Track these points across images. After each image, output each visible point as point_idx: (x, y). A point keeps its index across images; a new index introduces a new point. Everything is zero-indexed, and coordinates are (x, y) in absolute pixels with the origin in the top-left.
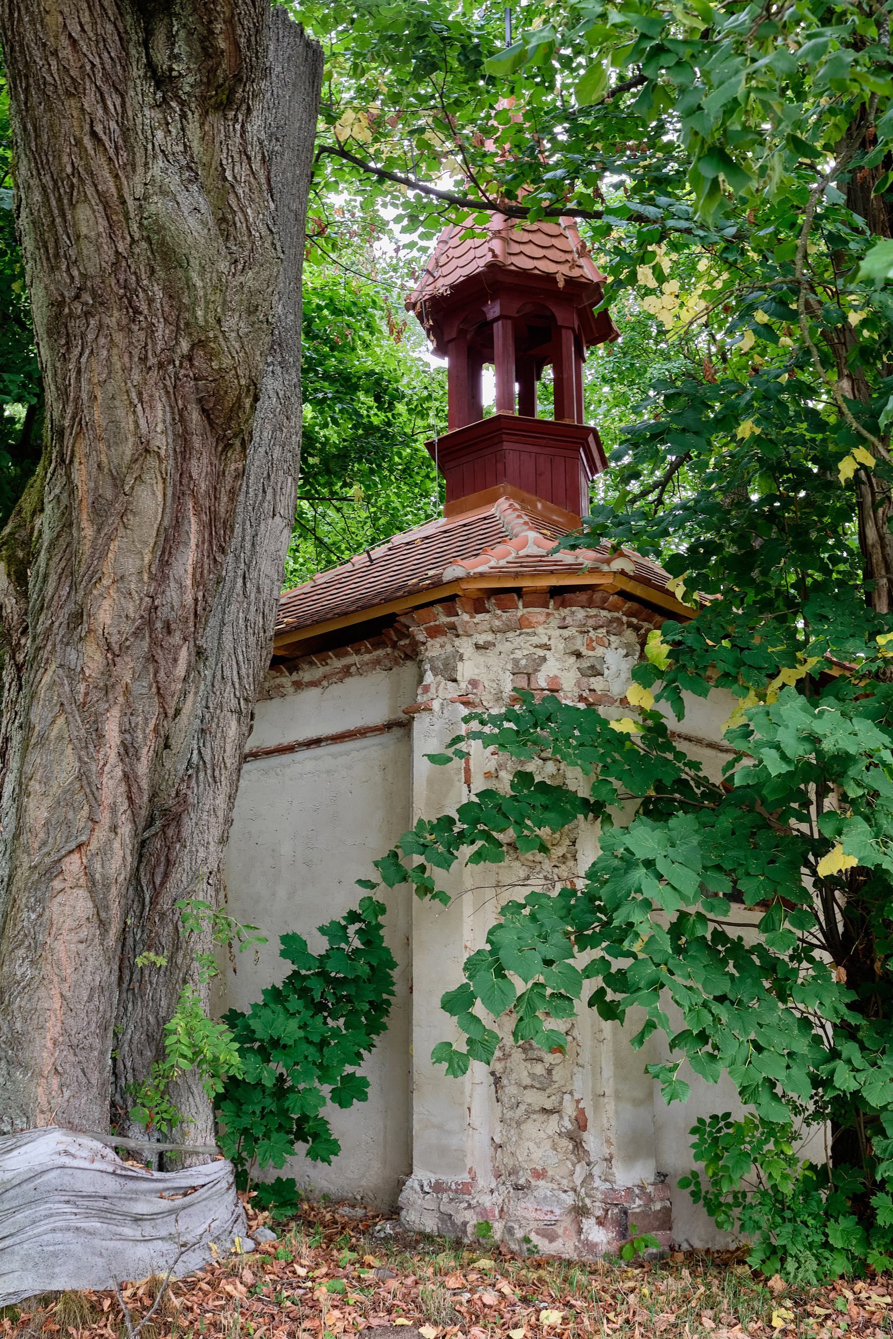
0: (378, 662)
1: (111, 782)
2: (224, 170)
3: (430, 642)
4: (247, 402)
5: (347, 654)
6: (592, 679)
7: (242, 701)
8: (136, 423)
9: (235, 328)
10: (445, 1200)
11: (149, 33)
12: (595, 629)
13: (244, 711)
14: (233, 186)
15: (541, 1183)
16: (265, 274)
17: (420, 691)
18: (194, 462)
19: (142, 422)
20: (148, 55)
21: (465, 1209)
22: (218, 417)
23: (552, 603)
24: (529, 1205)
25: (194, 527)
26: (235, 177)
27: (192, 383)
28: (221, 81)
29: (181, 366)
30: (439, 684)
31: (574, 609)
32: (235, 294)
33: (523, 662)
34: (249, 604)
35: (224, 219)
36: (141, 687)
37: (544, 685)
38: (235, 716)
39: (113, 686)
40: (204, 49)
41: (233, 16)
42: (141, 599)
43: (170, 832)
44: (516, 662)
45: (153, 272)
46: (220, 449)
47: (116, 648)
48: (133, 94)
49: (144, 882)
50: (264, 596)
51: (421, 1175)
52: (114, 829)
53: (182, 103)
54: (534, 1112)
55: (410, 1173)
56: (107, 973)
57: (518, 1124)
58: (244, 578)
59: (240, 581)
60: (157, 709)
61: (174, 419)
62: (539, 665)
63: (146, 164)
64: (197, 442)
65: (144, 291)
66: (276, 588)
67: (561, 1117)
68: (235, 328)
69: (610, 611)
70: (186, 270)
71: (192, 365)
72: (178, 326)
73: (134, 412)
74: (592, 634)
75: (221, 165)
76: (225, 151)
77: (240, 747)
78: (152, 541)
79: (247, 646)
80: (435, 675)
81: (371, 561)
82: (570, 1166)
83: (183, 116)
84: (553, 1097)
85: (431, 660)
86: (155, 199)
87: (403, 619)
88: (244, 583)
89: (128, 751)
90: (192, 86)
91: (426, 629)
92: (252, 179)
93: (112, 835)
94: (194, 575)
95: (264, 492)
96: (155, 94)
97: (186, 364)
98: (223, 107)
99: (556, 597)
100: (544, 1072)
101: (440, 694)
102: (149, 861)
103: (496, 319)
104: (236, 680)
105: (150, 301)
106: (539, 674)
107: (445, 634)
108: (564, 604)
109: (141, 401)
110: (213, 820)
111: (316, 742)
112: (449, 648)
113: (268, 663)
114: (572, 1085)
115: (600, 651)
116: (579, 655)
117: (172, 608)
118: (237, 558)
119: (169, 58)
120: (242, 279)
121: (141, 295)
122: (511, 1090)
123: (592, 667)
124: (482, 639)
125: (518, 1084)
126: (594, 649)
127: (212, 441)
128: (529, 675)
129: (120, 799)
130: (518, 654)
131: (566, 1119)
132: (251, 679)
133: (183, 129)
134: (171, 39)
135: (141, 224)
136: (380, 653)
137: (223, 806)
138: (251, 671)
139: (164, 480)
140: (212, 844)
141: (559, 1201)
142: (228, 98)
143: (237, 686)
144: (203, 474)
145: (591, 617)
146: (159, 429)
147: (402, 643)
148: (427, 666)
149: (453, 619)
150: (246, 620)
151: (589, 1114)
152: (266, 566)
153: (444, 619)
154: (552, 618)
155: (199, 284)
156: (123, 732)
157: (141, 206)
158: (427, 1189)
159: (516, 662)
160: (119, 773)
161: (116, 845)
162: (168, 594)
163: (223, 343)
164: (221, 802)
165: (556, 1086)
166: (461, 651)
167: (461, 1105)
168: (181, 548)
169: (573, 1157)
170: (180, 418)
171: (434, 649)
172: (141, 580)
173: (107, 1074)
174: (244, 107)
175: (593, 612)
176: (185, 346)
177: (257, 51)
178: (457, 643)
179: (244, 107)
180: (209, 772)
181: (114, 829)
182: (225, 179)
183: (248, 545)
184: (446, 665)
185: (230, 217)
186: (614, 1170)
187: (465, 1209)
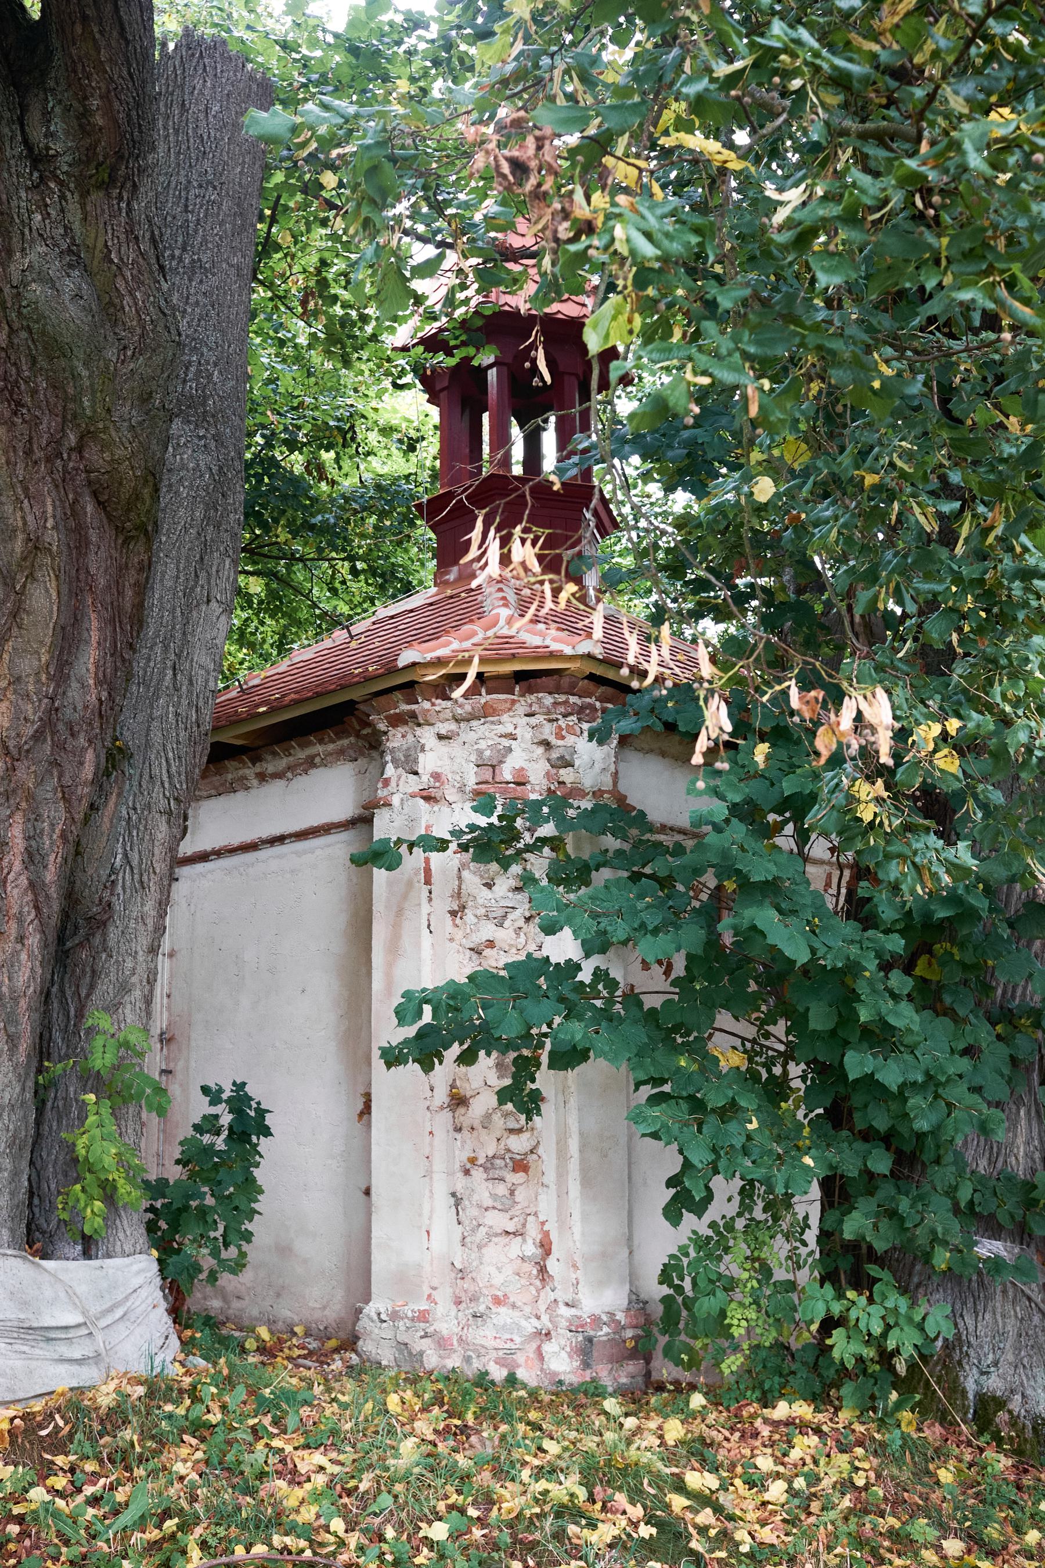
0: (341, 752)
1: (16, 891)
2: (110, 252)
3: (392, 731)
4: (146, 492)
5: (309, 744)
6: (562, 771)
7: (172, 802)
8: (23, 518)
9: (127, 417)
10: (402, 1328)
11: (24, 108)
12: (565, 716)
13: (175, 812)
14: (119, 268)
15: (502, 1310)
16: (158, 360)
17: (380, 785)
18: (92, 557)
19: (30, 518)
20: (23, 131)
21: (422, 1337)
22: (116, 510)
23: (517, 688)
24: (488, 1333)
25: (95, 624)
26: (121, 259)
27: (83, 475)
28: (101, 159)
29: (69, 459)
30: (399, 778)
31: (541, 695)
32: (125, 382)
33: (488, 753)
34: (180, 697)
35: (111, 303)
36: (48, 790)
37: (509, 777)
38: (164, 818)
39: (14, 791)
40: (80, 126)
41: (109, 92)
42: (40, 701)
43: (97, 940)
44: (480, 753)
45: (34, 361)
46: (120, 541)
47: (14, 752)
48: (6, 175)
49: (69, 993)
50: (198, 687)
51: (377, 1305)
52: (21, 939)
53: (61, 183)
54: (496, 1235)
55: (367, 1299)
56: (18, 1090)
57: (480, 1247)
58: (174, 669)
59: (169, 673)
60: (63, 815)
61: (65, 514)
62: (505, 756)
63: (23, 250)
64: (93, 536)
65: (26, 382)
66: (211, 679)
67: (524, 1241)
68: (127, 417)
69: (580, 697)
70: (70, 359)
71: (82, 458)
72: (64, 417)
73: (21, 509)
74: (562, 723)
75: (106, 246)
76: (110, 232)
77: (173, 849)
78: (48, 640)
79: (178, 742)
80: (396, 768)
81: (351, 637)
82: (534, 1292)
83: (62, 197)
84: (516, 1219)
85: (393, 751)
86: (34, 286)
87: (362, 707)
88: (175, 675)
89: (33, 858)
90: (70, 165)
91: (386, 718)
92: (141, 260)
93: (19, 946)
94: (96, 674)
95: (197, 576)
96: (31, 174)
97: (74, 456)
98: (105, 186)
99: (523, 683)
100: (507, 1193)
101: (400, 788)
102: (74, 971)
103: (490, 366)
104: (165, 778)
105: (34, 392)
106: (504, 766)
107: (406, 723)
108: (531, 691)
109: (27, 496)
110: (141, 927)
111: (280, 839)
112: (410, 738)
113: (205, 759)
114: (536, 1206)
115: (570, 740)
116: (547, 744)
117: (75, 709)
118: (166, 648)
119: (46, 136)
120: (132, 365)
121: (23, 387)
122: (470, 1212)
123: (562, 758)
124: (444, 728)
125: (479, 1206)
126: (563, 738)
127: (110, 532)
128: (493, 767)
129: (26, 909)
130: (483, 745)
131: (530, 1241)
132: (183, 777)
133: (62, 211)
134: (47, 117)
135: (20, 313)
136: (345, 742)
137: (153, 913)
138: (183, 769)
139: (57, 577)
140: (141, 953)
141: (519, 1327)
142: (110, 176)
143: (167, 785)
144: (102, 570)
145: (560, 703)
146: (49, 525)
147: (364, 732)
148: (388, 758)
149: (414, 707)
150: (177, 714)
151: (554, 1237)
152: (202, 658)
153: (405, 707)
154: (517, 705)
155: (85, 373)
156: (28, 838)
157: (19, 294)
158: (383, 1317)
159: (480, 753)
160: (23, 881)
161: (24, 956)
162: (70, 694)
163: (113, 434)
164: (150, 908)
165: (519, 1207)
166: (422, 741)
167: (420, 1227)
168: (82, 647)
169: (538, 1283)
170: (74, 511)
171: (397, 740)
172: (38, 681)
173: (22, 1195)
174: (129, 185)
175: (562, 698)
176: (72, 438)
177: (140, 126)
178: (418, 733)
179: (129, 185)
180: (136, 877)
181: (21, 939)
182: (111, 261)
183: (178, 635)
184: (407, 756)
185: (117, 301)
186: (580, 1296)
187: (422, 1337)
